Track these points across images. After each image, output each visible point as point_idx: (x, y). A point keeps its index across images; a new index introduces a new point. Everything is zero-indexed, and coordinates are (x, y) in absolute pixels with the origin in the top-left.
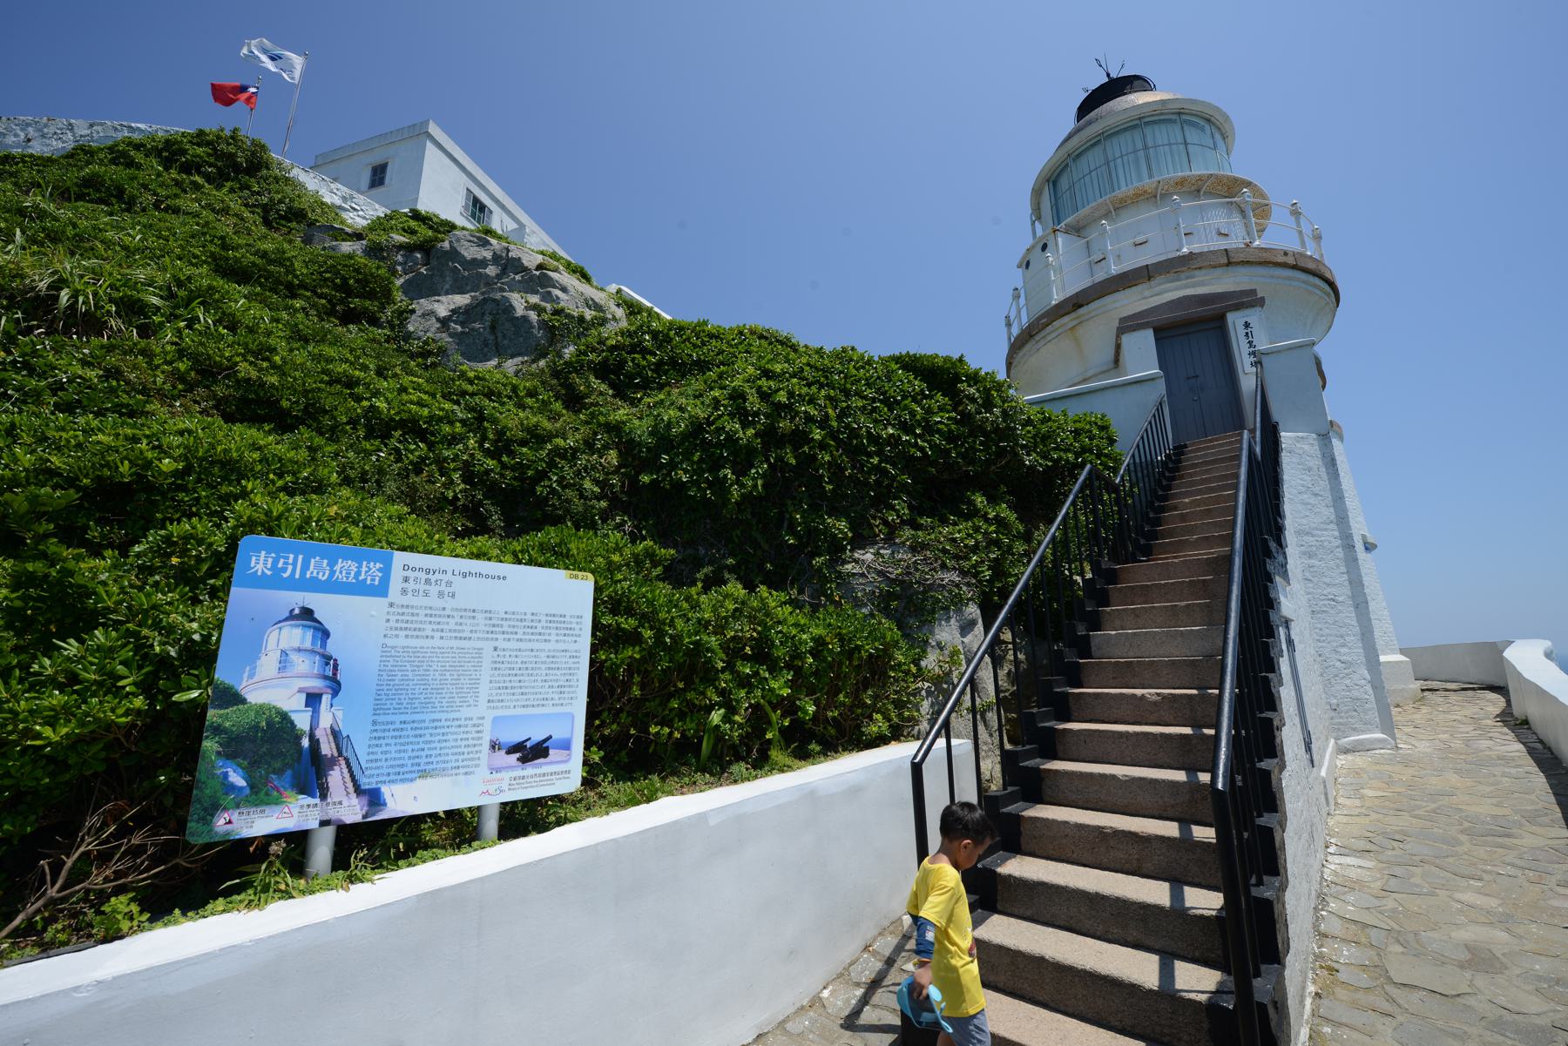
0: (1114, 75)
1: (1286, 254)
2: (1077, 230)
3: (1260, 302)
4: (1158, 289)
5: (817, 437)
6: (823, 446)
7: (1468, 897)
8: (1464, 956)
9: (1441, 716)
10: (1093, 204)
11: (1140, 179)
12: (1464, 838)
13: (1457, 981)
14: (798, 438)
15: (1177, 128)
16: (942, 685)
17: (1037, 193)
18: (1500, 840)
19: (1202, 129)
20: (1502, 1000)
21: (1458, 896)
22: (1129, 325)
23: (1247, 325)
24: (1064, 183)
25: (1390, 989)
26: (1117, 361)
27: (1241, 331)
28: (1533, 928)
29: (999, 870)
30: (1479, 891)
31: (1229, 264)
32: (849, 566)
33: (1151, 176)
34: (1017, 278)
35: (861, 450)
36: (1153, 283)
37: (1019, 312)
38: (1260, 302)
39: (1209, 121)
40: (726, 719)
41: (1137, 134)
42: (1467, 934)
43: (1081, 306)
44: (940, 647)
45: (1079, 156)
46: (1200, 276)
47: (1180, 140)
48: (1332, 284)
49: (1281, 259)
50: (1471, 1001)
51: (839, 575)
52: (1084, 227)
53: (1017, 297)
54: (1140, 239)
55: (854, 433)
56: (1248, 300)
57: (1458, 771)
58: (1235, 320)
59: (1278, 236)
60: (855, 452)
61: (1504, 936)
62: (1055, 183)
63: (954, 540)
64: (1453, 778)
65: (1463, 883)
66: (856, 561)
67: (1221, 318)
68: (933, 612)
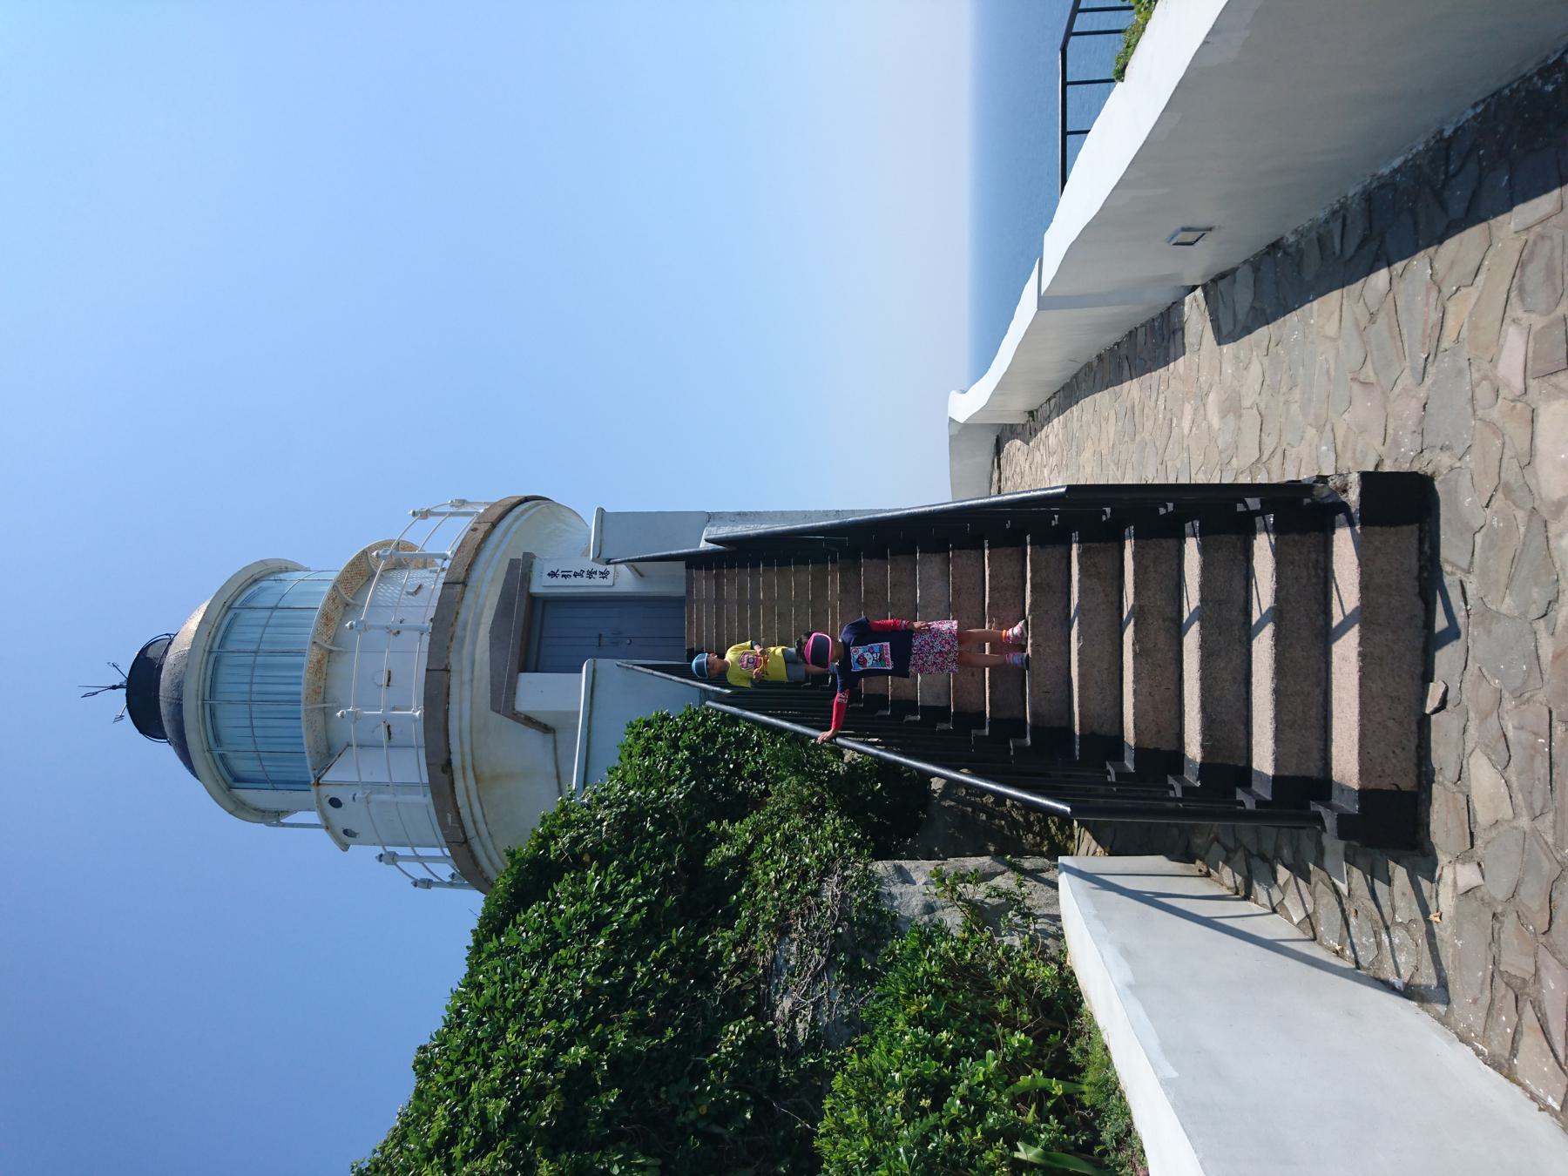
0: (122, 680)
1: (474, 530)
2: (328, 754)
3: (529, 559)
4: (466, 663)
5: (582, 1051)
6: (600, 1045)
7: (1186, 424)
8: (1231, 417)
9: (1027, 479)
10: (304, 725)
11: (300, 667)
12: (1138, 438)
13: (1251, 420)
14: (579, 1083)
15: (246, 614)
16: (982, 916)
17: (240, 809)
18: (1137, 413)
19: (263, 590)
20: (1257, 387)
21: (1186, 431)
22: (503, 699)
23: (553, 574)
24: (243, 766)
25: (1264, 458)
26: (546, 729)
27: (560, 581)
28: (1202, 379)
29: (1199, 760)
30: (1180, 419)
31: (464, 583)
32: (800, 1026)
33: (300, 653)
34: (364, 854)
35: (618, 992)
36: (454, 667)
37: (418, 858)
38: (529, 559)
39: (255, 581)
40: (1031, 1141)
41: (228, 660)
42: (1215, 420)
43: (449, 762)
44: (930, 909)
45: (217, 738)
46: (466, 614)
47: (267, 613)
48: (527, 499)
49: (479, 535)
50: (1262, 406)
51: (813, 1045)
52: (329, 747)
53: (393, 859)
54: (384, 681)
55: (592, 994)
56: (521, 570)
57: (1078, 454)
58: (541, 585)
59: (445, 538)
60: (619, 999)
61: (1212, 397)
62: (237, 779)
63: (779, 882)
64: (1087, 455)
65: (1175, 430)
66: (794, 1014)
67: (533, 600)
68: (880, 914)
